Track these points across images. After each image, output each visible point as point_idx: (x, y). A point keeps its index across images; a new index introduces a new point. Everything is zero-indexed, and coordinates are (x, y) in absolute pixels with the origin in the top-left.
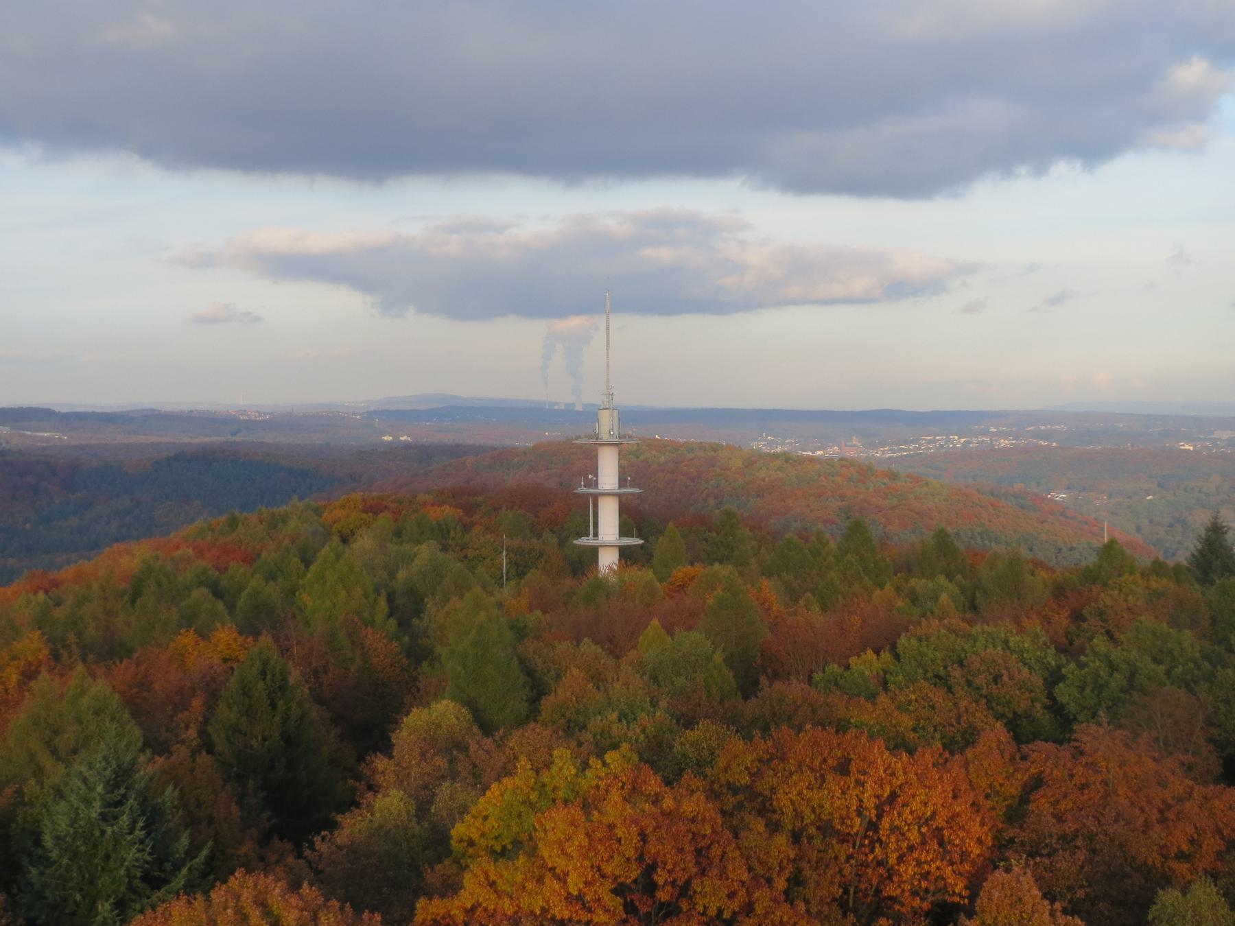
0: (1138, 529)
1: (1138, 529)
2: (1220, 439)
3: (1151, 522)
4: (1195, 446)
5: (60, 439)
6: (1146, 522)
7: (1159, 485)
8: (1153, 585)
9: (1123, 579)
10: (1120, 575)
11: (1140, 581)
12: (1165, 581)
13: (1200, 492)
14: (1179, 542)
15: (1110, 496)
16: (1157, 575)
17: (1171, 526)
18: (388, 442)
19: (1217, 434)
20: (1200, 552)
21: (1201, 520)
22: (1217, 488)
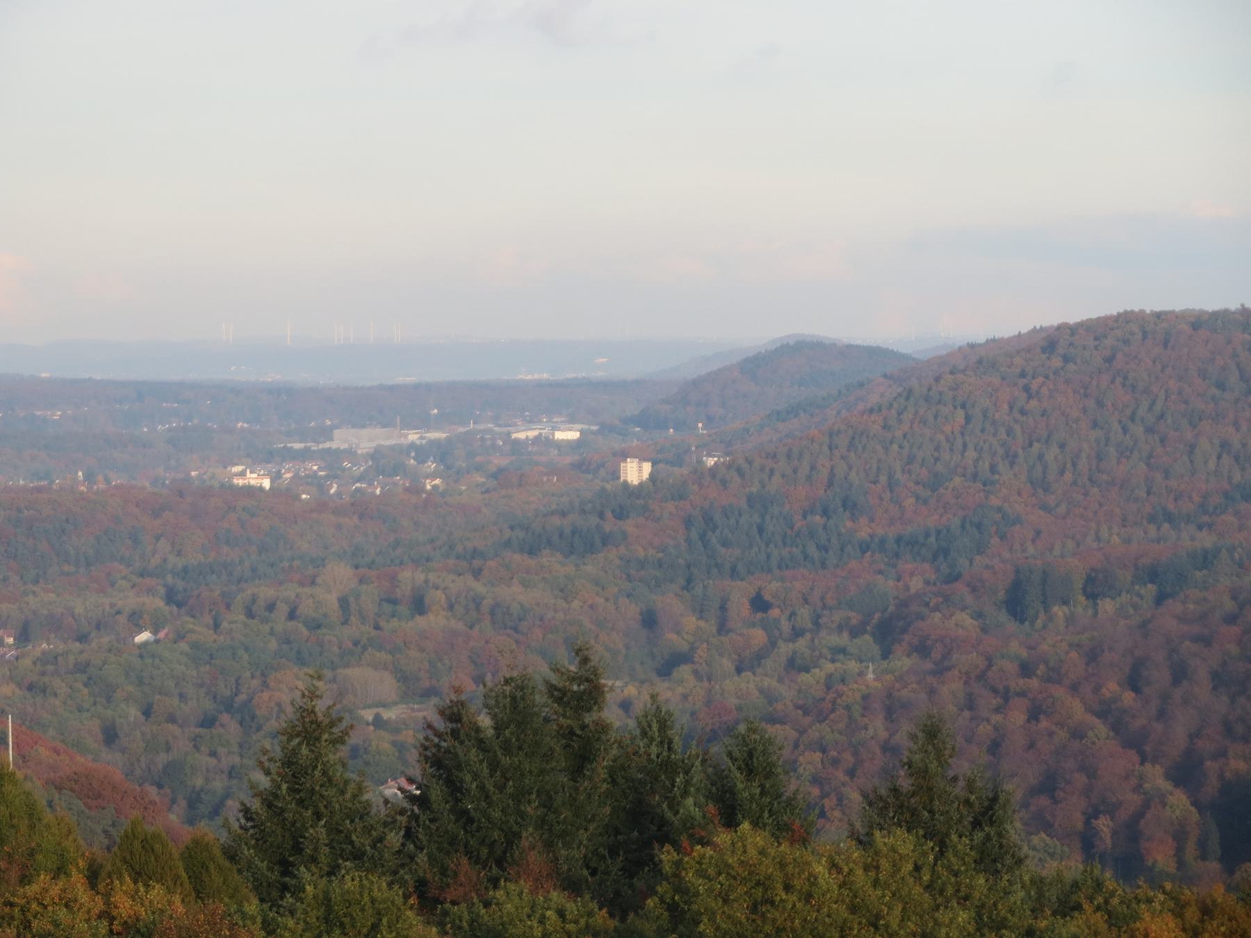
0: (110, 736)
1: (110, 736)
2: (350, 453)
3: (147, 713)
4: (275, 477)
5: (545, 443)
6: (134, 713)
7: (170, 597)
8: (124, 906)
9: (32, 889)
10: (25, 880)
11: (83, 895)
12: (157, 892)
13: (292, 615)
14: (231, 773)
15: (24, 636)
16: (137, 876)
17: (208, 722)
18: (252, 492)
19: (341, 439)
20: (270, 800)
21: (283, 694)
22: (344, 602)
